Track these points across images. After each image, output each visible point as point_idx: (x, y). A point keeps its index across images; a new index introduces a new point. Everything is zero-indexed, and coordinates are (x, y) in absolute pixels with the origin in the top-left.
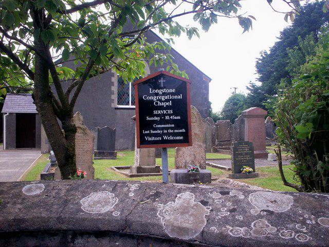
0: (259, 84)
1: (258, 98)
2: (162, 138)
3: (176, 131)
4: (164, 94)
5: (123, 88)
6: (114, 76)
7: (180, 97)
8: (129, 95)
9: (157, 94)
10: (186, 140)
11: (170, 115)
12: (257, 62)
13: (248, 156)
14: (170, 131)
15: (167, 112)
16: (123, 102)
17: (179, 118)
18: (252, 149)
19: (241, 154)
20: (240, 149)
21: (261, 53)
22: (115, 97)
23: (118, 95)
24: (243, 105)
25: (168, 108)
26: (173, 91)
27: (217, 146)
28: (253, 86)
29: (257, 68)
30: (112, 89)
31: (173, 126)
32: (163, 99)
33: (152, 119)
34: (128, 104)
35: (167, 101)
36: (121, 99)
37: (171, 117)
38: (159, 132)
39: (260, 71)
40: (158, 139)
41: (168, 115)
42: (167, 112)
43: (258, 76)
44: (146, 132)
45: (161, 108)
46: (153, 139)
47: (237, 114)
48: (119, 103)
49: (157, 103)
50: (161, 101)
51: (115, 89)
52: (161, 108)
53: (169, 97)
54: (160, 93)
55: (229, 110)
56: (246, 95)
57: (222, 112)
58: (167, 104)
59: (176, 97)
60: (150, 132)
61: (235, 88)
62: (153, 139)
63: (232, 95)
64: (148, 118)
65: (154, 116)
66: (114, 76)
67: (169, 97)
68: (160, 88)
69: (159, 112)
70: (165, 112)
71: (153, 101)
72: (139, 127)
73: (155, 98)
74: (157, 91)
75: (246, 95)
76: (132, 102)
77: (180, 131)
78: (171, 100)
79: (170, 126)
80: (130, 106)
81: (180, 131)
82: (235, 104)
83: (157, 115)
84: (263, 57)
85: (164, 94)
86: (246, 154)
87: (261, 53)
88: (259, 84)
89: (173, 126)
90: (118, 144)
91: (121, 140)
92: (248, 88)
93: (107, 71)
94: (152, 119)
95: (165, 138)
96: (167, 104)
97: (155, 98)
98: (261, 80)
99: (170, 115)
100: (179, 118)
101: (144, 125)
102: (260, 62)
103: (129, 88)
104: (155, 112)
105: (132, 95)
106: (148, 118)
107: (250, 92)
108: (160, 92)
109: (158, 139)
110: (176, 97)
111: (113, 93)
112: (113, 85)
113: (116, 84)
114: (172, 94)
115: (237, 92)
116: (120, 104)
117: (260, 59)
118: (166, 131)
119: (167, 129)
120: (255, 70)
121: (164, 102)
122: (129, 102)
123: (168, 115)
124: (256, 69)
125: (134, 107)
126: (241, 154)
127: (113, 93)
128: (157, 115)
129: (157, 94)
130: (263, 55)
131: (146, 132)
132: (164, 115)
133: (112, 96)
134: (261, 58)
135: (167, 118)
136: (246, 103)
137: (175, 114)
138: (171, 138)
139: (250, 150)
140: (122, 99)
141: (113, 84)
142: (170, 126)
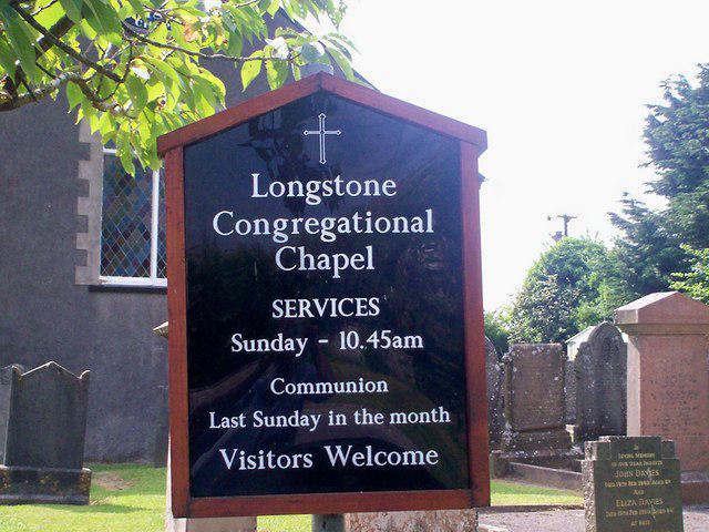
0: (659, 205)
1: (654, 258)
2: (321, 458)
3: (398, 418)
4: (333, 206)
5: (127, 206)
6: (87, 158)
7: (425, 224)
8: (148, 236)
9: (296, 207)
10: (87, 231)
11: (366, 326)
12: (652, 119)
13: (658, 501)
14: (367, 418)
15: (349, 307)
16: (126, 264)
17: (416, 342)
18: (670, 470)
19: (626, 493)
20: (623, 469)
21: (665, 85)
22: (90, 242)
23: (105, 234)
24: (596, 284)
25: (353, 284)
26: (385, 188)
27: (509, 449)
28: (636, 213)
29: (652, 142)
30: (80, 212)
31: (382, 386)
32: (328, 236)
33: (263, 345)
34: (143, 270)
35: (348, 244)
36: (116, 249)
37: (374, 339)
38: (301, 420)
39: (661, 155)
40: (293, 462)
41: (355, 323)
42: (349, 307)
43: (655, 174)
44: (226, 423)
45: (319, 285)
46: (265, 461)
47: (575, 319)
48: (107, 268)
49: (290, 258)
50: (315, 246)
51: (91, 208)
52: (319, 285)
53: (362, 225)
54: (313, 199)
55: (544, 303)
56: (610, 246)
57: (515, 313)
58: (351, 261)
59: (397, 225)
60: (250, 420)
61: (567, 219)
62: (265, 461)
63: (553, 243)
64: (239, 344)
65: (268, 328)
66: (87, 158)
67: (362, 225)
68: (309, 173)
69: (305, 308)
70: (336, 307)
71: (263, 247)
72: (185, 442)
73: (278, 231)
74: (293, 188)
75: (610, 246)
76: (160, 265)
77: (423, 417)
78: (374, 239)
79: (362, 387)
80: (154, 280)
81: (423, 417)
82: (566, 270)
83: (291, 328)
84: (676, 104)
85: (333, 206)
86: (650, 492)
87: (665, 85)
88: (659, 205)
89: (382, 386)
90: (95, 438)
91: (114, 421)
92: (616, 220)
93: (33, 97)
94: (263, 345)
95: (337, 455)
96: (351, 261)
97: (278, 231)
98: (669, 188)
99: (366, 326)
100: (416, 342)
101: (206, 356)
102: (662, 119)
103: (149, 207)
104: (282, 309)
105: (161, 236)
106: (239, 344)
107: (623, 234)
108: (312, 194)
109: (293, 462)
110: (397, 225)
111: (82, 225)
112: (86, 194)
113: (97, 189)
114: (383, 207)
115: (575, 233)
116: (111, 273)
117: (660, 110)
118: (338, 420)
119: (349, 403)
120: (642, 149)
121: (331, 249)
122: (147, 264)
123: (355, 323)
124: (648, 148)
125: (163, 283)
126: (626, 493)
127: (82, 225)
128: (291, 328)
129: (296, 207)
130: (675, 94)
131: (226, 423)
132: (330, 326)
133: (80, 237)
134: (667, 104)
135: (348, 340)
136: (610, 274)
137: (391, 320)
138: (371, 458)
139: (664, 474)
140: (121, 249)
141: (82, 188)
142: (362, 387)
